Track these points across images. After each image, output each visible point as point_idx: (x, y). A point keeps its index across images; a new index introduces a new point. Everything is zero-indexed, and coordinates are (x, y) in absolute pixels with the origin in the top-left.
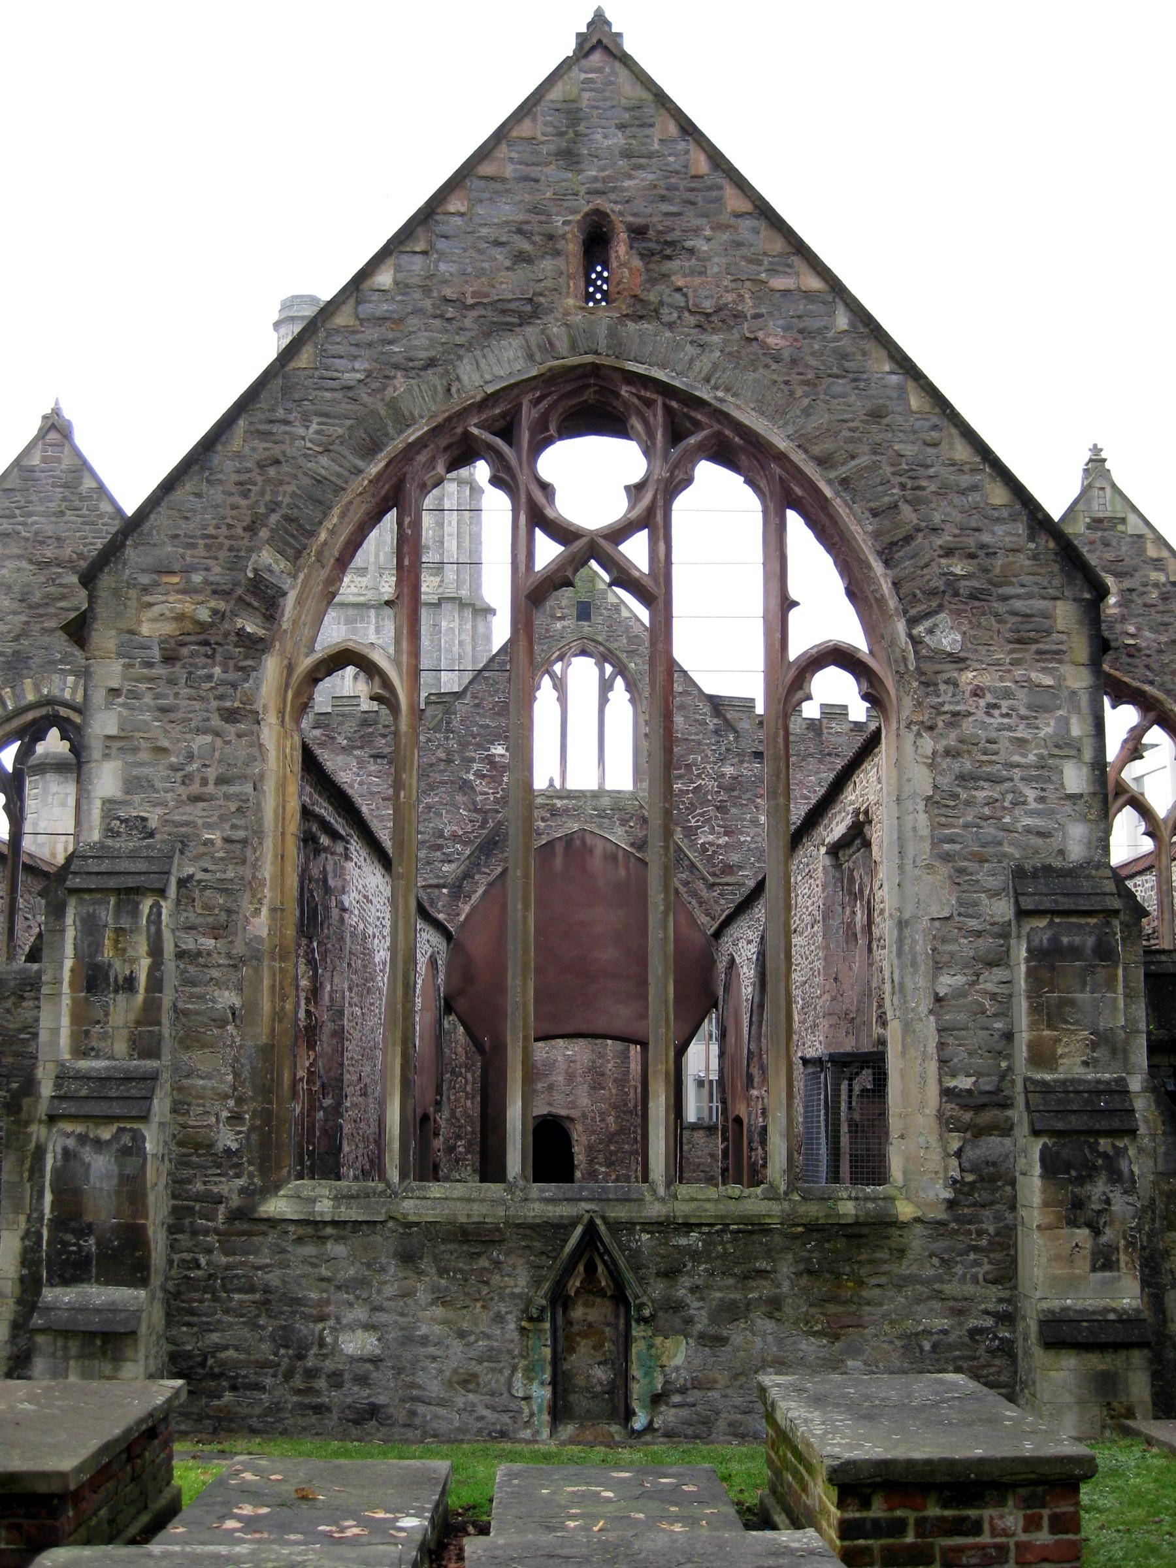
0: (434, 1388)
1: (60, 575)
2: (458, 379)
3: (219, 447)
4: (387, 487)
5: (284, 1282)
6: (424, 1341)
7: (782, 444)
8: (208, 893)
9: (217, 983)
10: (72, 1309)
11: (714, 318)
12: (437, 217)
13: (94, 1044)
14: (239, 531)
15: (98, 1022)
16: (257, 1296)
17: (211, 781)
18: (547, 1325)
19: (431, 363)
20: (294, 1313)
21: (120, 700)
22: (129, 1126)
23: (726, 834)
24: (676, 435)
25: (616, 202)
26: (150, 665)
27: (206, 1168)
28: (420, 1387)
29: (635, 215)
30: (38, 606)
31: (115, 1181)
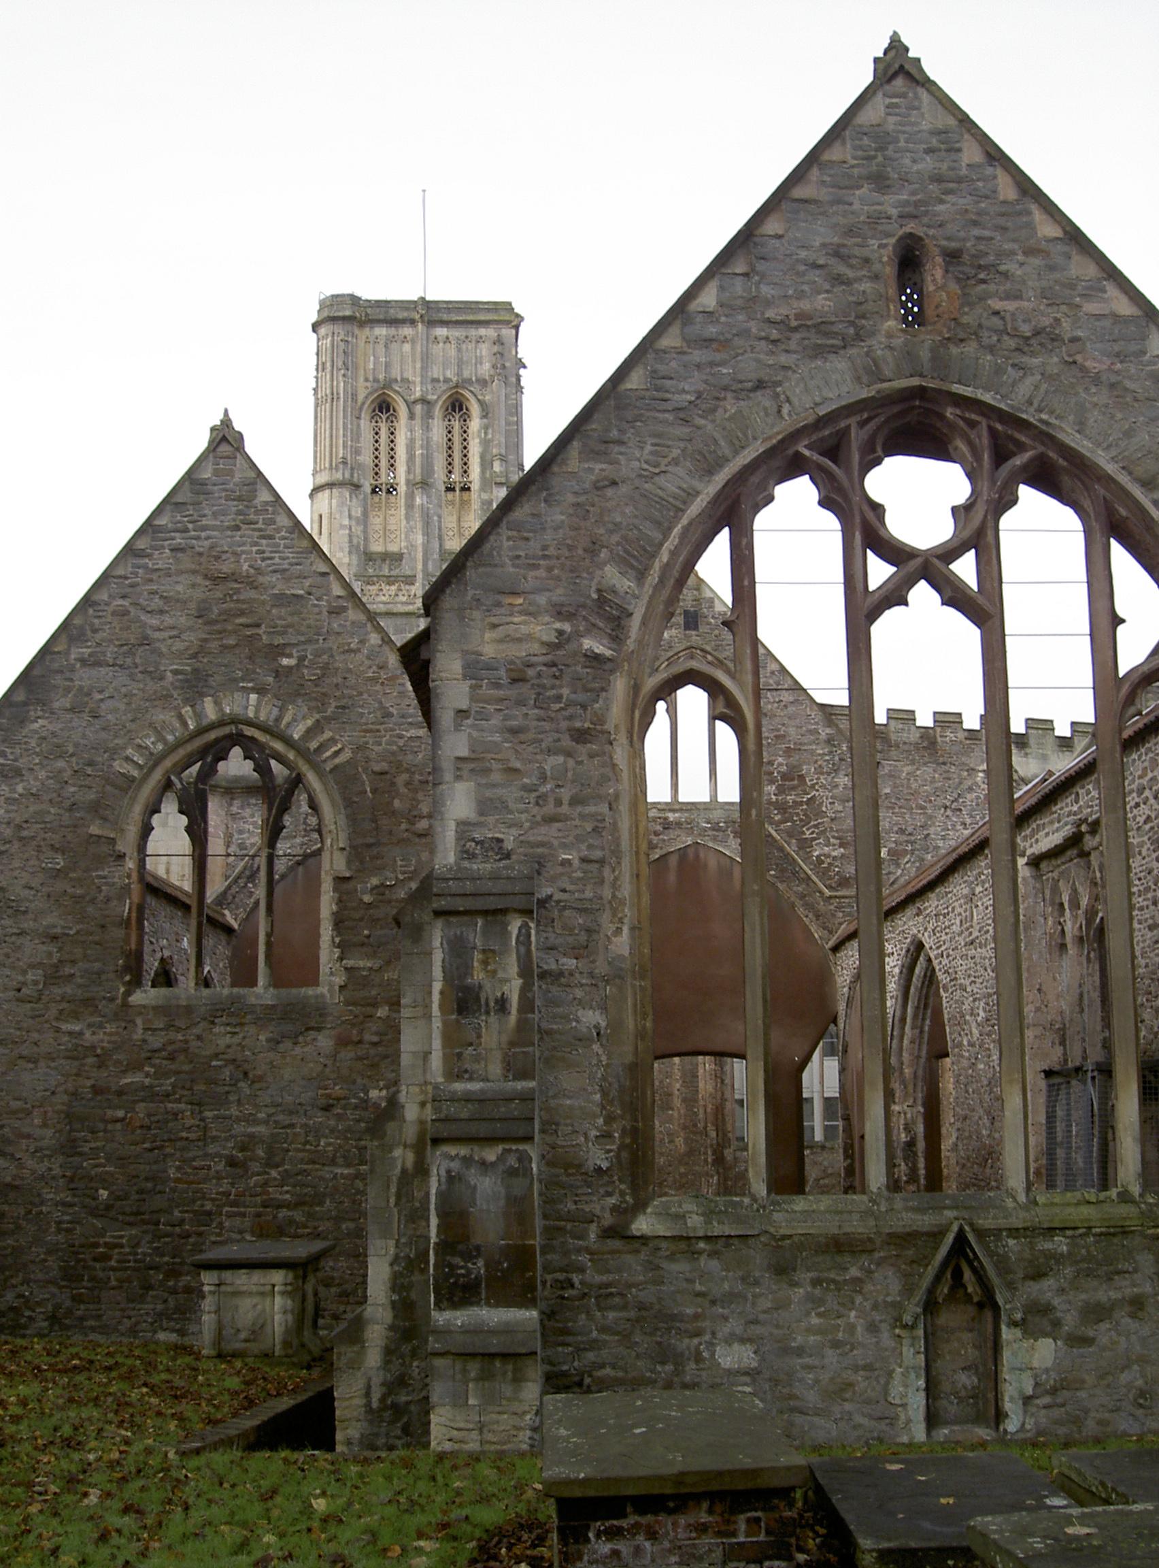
0: (812, 1398)
1: (238, 591)
2: (788, 400)
3: (555, 469)
4: (722, 508)
5: (660, 1299)
6: (800, 1352)
7: (1110, 468)
8: (567, 913)
9: (580, 1003)
10: (466, 1330)
11: (1033, 341)
12: (756, 239)
13: (467, 1066)
14: (580, 552)
15: (471, 1044)
16: (632, 1314)
17: (566, 800)
18: (921, 1332)
19: (760, 385)
20: (669, 1329)
21: (469, 722)
22: (514, 1147)
23: (841, 845)
24: (1000, 457)
25: (929, 226)
26: (497, 686)
27: (578, 1187)
28: (797, 1398)
29: (948, 239)
30: (216, 622)
31: (502, 1202)
